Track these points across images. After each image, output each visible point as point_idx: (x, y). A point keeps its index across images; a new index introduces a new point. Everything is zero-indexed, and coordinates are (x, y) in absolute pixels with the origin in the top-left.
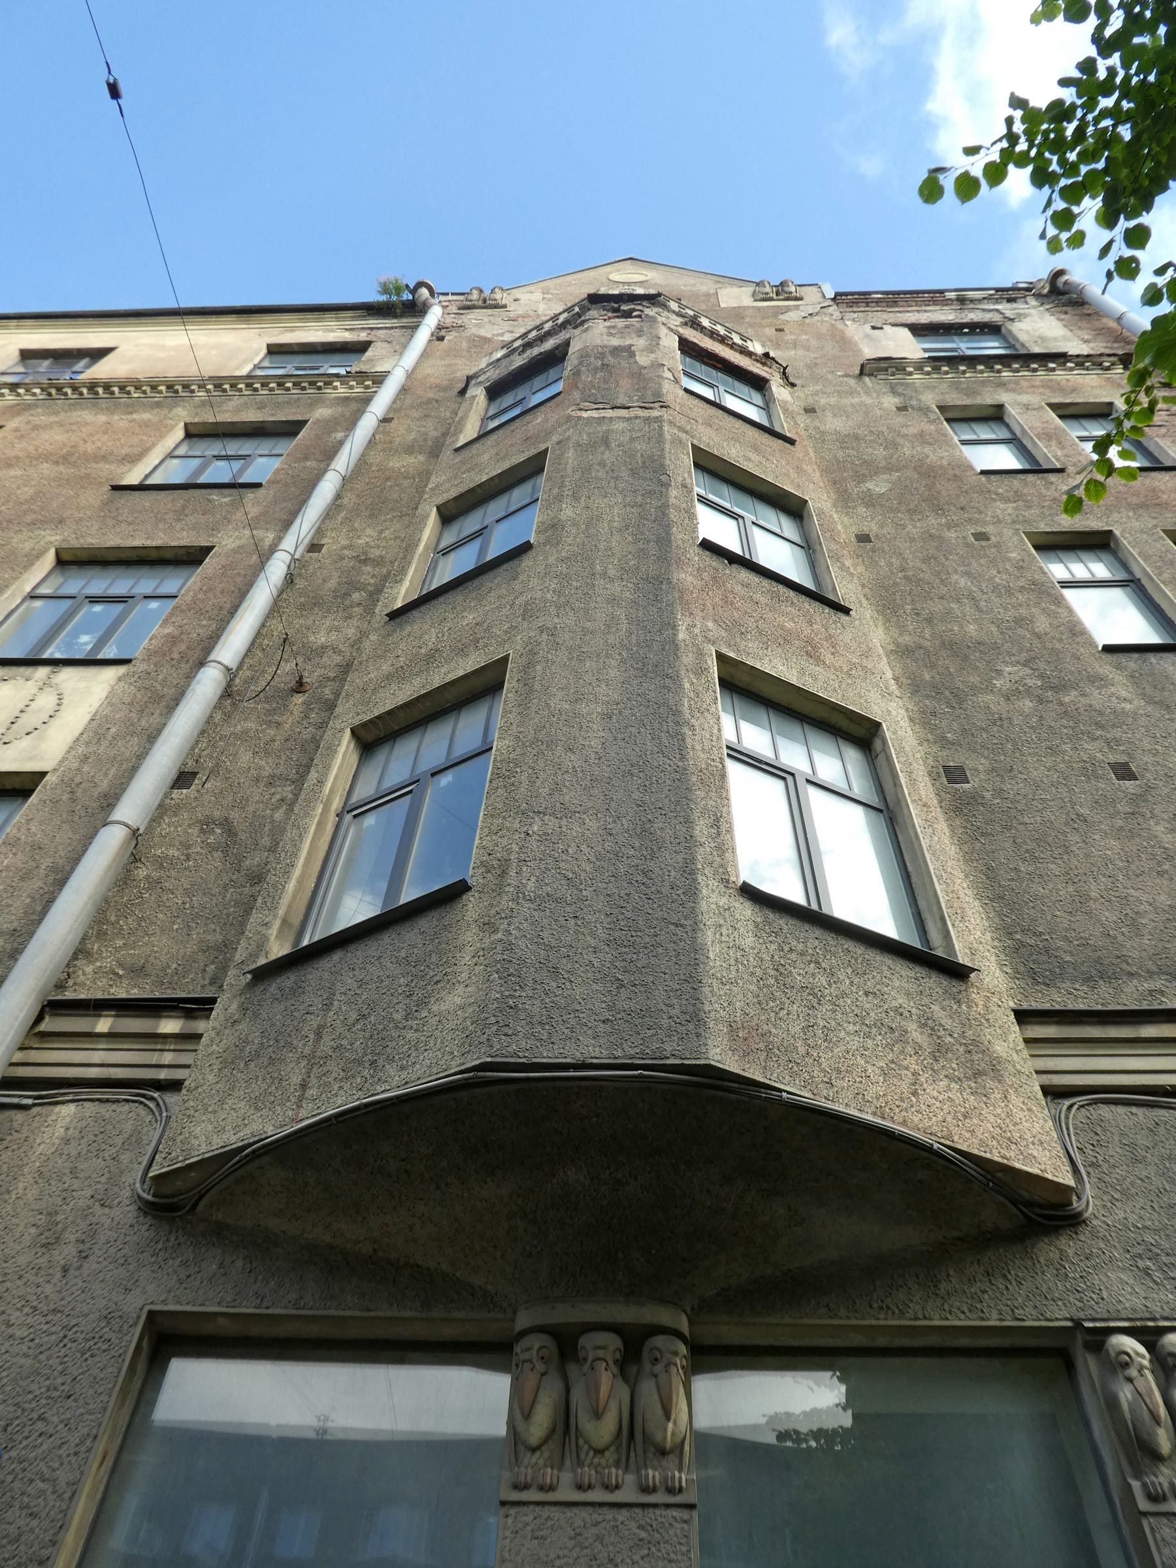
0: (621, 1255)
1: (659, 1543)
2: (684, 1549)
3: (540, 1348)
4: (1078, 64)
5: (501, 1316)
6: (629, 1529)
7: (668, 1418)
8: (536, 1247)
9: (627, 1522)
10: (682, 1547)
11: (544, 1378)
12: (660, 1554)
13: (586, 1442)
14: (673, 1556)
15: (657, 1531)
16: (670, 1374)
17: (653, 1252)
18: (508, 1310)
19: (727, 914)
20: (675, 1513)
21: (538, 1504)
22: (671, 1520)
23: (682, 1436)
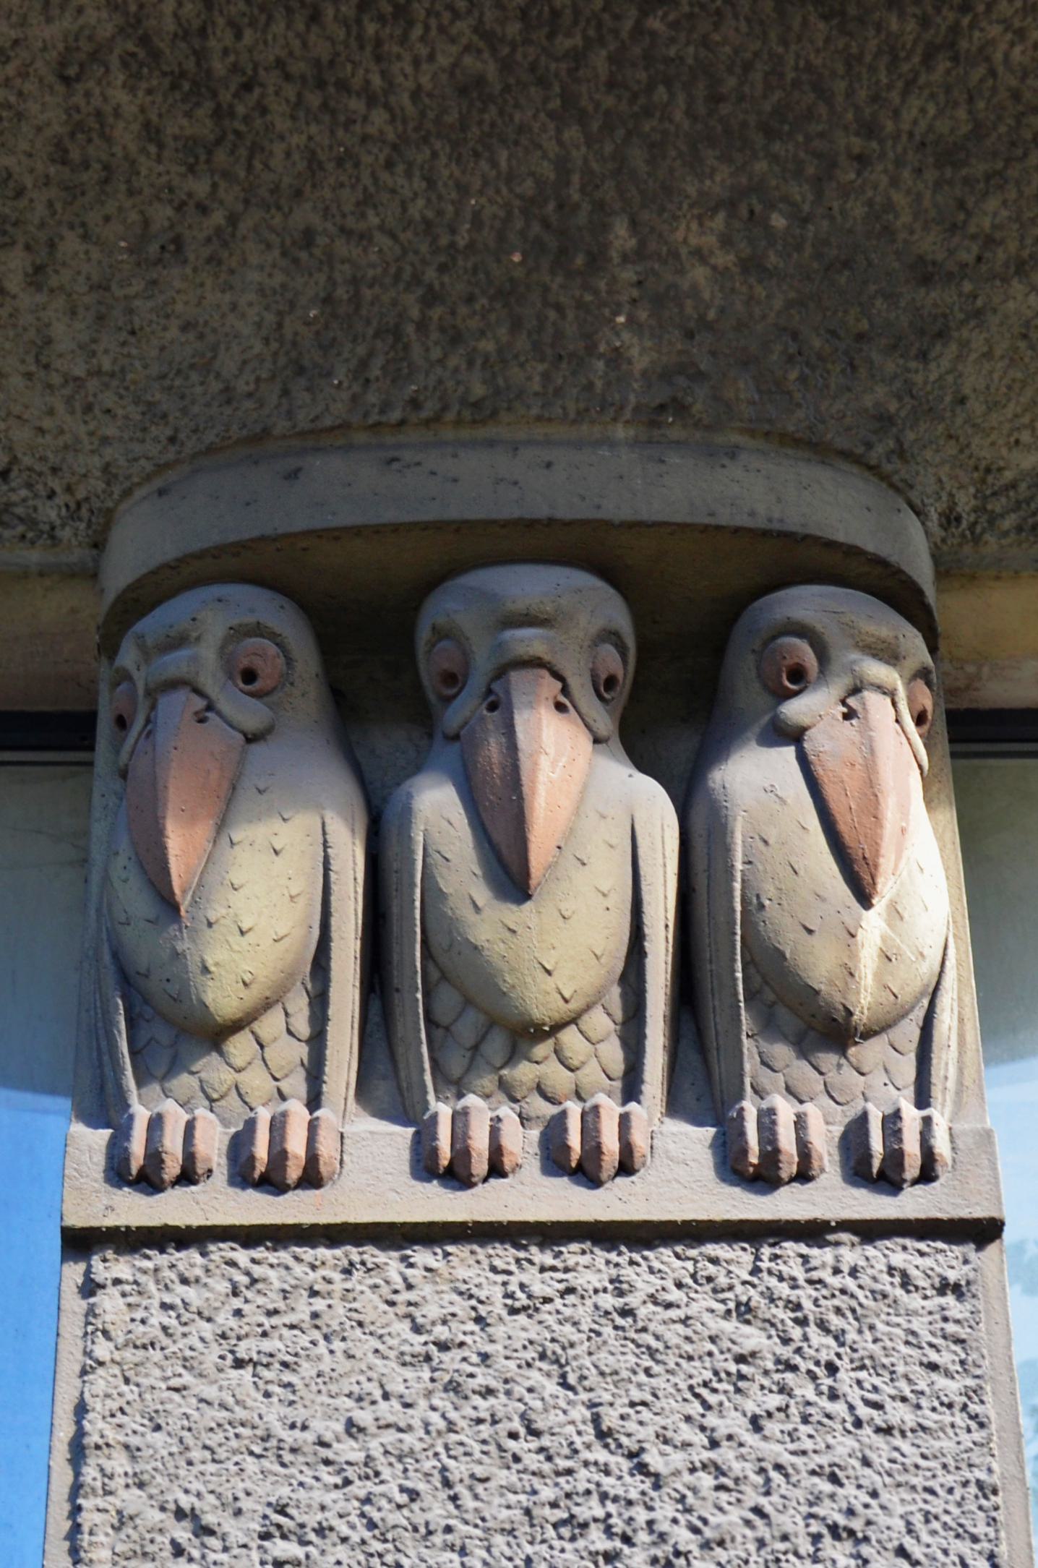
0: (621, 236)
1: (832, 1369)
2: (952, 1387)
3: (239, 633)
4: (1003, 1224)
5: (34, 556)
6: (685, 1321)
7: (865, 899)
8: (203, 209)
9: (675, 1295)
10: (941, 1381)
11: (256, 748)
12: (839, 1408)
13: (468, 1002)
14: (898, 1414)
15: (823, 1326)
16: (866, 728)
17: (778, 221)
18: (65, 534)
19: (522, 1299)
20: (901, 1253)
21: (249, 1236)
22: (888, 1284)
23: (928, 968)
